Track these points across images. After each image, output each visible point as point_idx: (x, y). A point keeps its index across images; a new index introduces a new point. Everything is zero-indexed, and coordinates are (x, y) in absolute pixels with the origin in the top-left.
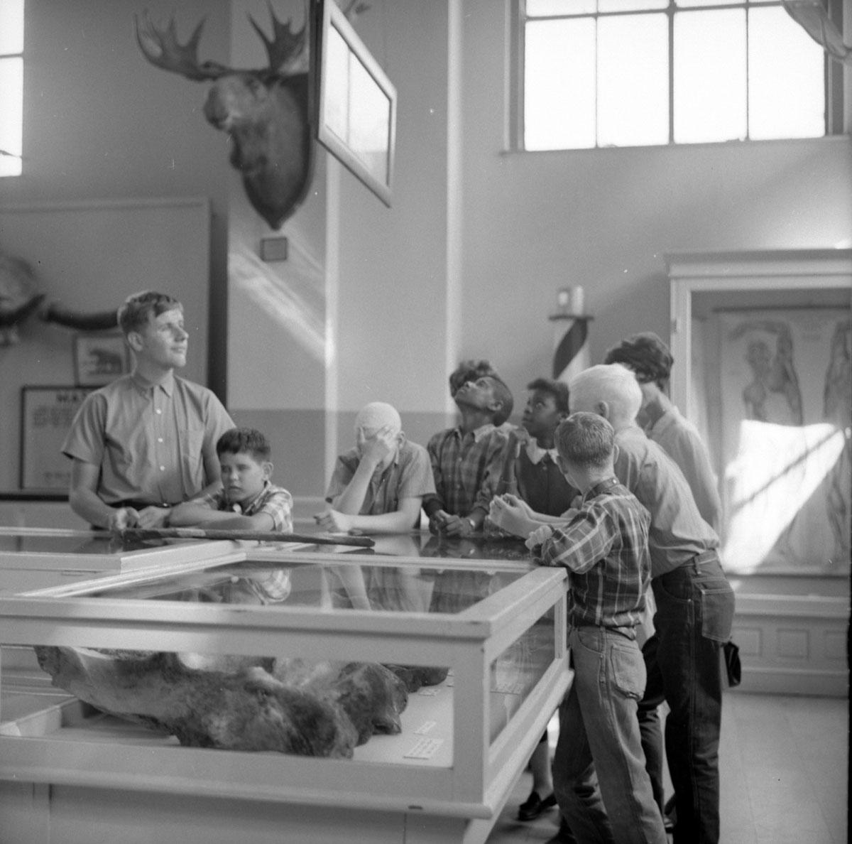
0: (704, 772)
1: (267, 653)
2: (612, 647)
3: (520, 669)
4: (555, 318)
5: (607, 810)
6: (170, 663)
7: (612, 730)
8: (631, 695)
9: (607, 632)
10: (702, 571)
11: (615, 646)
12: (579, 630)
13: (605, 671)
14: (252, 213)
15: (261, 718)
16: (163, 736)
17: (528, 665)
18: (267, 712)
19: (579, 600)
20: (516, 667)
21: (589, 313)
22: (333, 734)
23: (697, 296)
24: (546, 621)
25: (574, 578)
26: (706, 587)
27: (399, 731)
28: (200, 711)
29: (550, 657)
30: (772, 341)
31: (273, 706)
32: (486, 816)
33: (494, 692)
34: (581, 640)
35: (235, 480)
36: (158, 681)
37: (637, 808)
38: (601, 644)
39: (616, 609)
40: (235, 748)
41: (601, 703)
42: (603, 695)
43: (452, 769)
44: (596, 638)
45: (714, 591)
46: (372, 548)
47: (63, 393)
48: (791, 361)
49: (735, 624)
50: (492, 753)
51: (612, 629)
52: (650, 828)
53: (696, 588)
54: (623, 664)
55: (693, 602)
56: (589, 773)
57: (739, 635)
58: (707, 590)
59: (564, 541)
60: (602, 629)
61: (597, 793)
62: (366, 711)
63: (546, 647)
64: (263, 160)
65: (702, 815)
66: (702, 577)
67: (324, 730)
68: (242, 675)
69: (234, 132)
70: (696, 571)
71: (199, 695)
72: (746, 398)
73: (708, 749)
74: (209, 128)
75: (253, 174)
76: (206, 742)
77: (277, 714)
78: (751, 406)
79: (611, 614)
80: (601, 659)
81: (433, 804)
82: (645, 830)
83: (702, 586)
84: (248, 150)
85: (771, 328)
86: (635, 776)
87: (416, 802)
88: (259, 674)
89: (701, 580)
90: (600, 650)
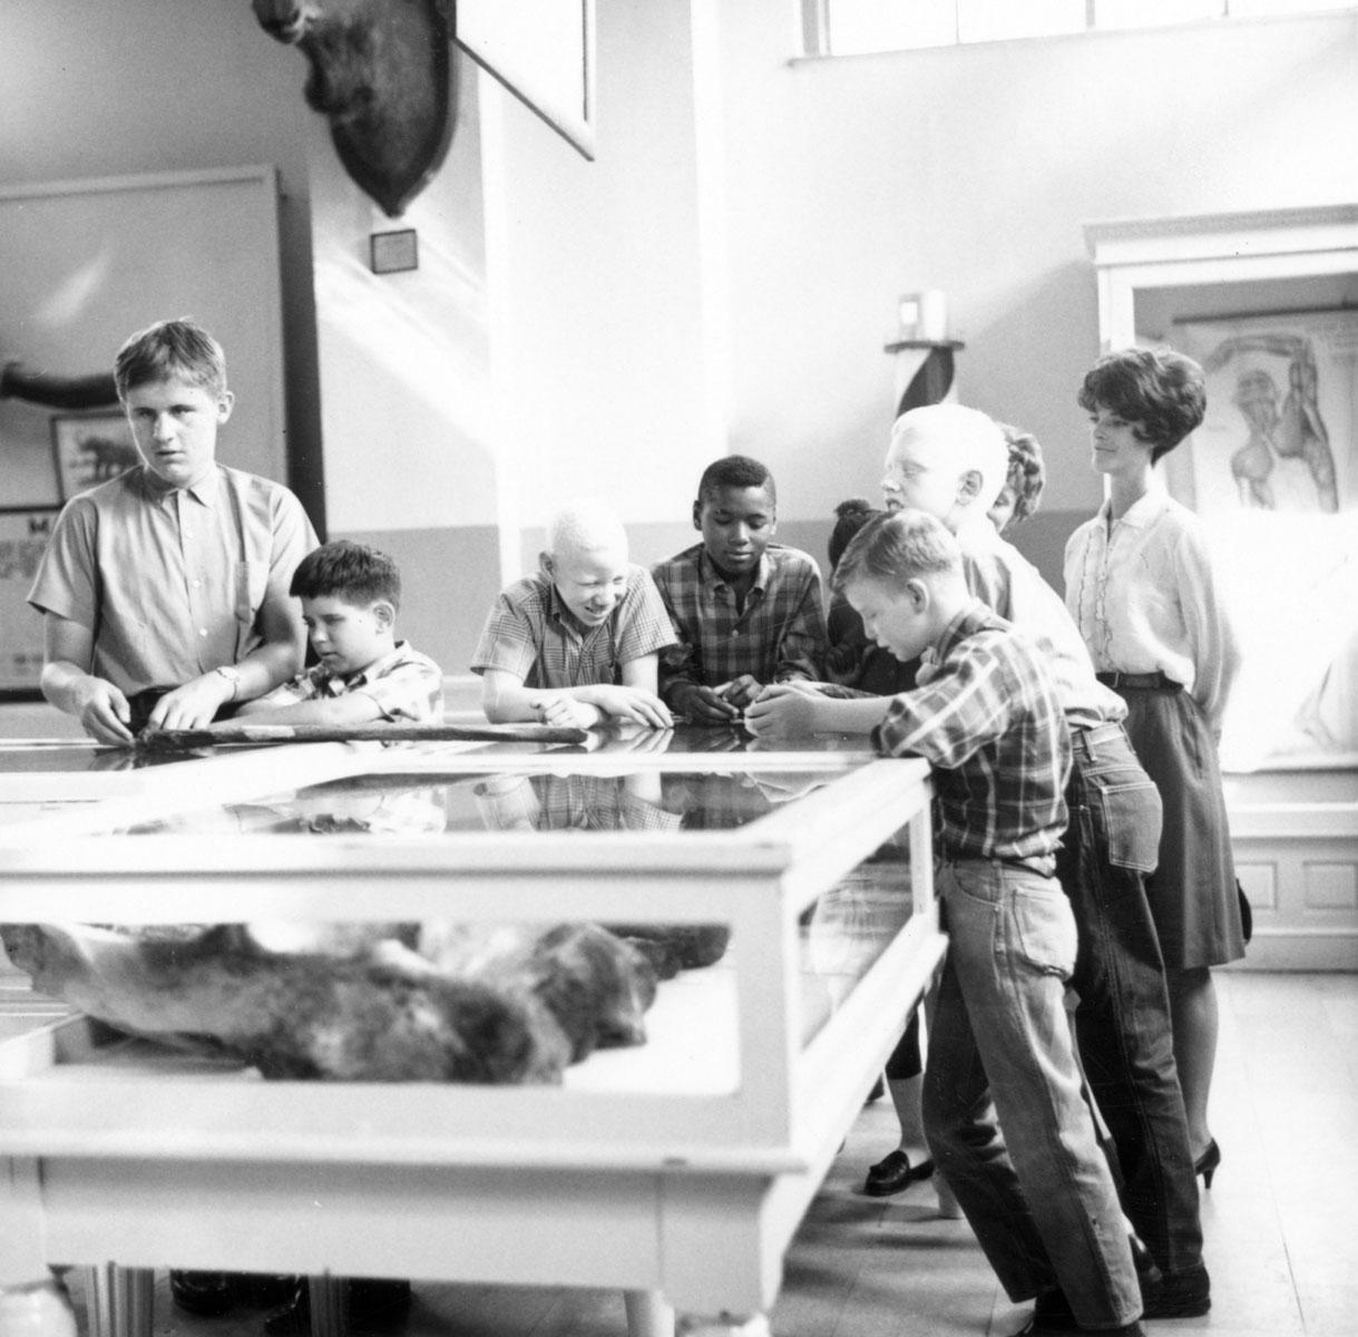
0: (1156, 1090)
1: (405, 914)
2: (1014, 894)
3: (853, 934)
4: (897, 348)
5: (1015, 1165)
6: (235, 940)
7: (1019, 1032)
8: (1051, 970)
9: (1004, 868)
10: (1099, 756)
11: (1020, 890)
12: (956, 867)
13: (1004, 932)
14: (352, 189)
15: (400, 1027)
16: (235, 1069)
17: (865, 930)
18: (410, 1016)
19: (954, 817)
20: (845, 934)
21: (955, 337)
22: (524, 1050)
23: (1144, 297)
24: (893, 854)
25: (941, 779)
26: (1107, 782)
27: (643, 1041)
28: (292, 1019)
29: (904, 914)
30: (1279, 370)
31: (421, 1004)
32: (800, 1170)
33: (808, 974)
34: (960, 884)
35: (322, 642)
36: (218, 977)
37: (1067, 1161)
38: (995, 889)
39: (1021, 830)
40: (359, 1078)
41: (998, 987)
42: (1002, 974)
43: (736, 1095)
44: (987, 879)
45: (1123, 788)
46: (583, 744)
47: (38, 518)
48: (1314, 403)
49: (1237, 855)
50: (803, 1069)
51: (1014, 862)
52: (1090, 1192)
53: (1091, 785)
54: (1034, 919)
55: (1088, 809)
56: (984, 1105)
57: (1251, 875)
58: (1109, 787)
59: (907, 715)
60: (996, 863)
61: (999, 1139)
62: (585, 1007)
63: (897, 897)
64: (365, 93)
65: (1163, 1164)
66: (1100, 765)
67: (511, 1042)
68: (362, 957)
69: (309, 45)
70: (1088, 756)
71: (290, 995)
72: (1238, 472)
73: (1156, 1051)
74: (268, 41)
75: (347, 119)
76: (307, 1070)
77: (428, 1018)
78: (1245, 483)
79: (1010, 840)
80: (997, 914)
81: (707, 1154)
82: (1083, 1197)
83: (1100, 780)
84: (336, 75)
85: (1277, 347)
86: (1064, 1110)
87: (676, 1150)
88: (394, 954)
89: (1097, 770)
90: (994, 899)
